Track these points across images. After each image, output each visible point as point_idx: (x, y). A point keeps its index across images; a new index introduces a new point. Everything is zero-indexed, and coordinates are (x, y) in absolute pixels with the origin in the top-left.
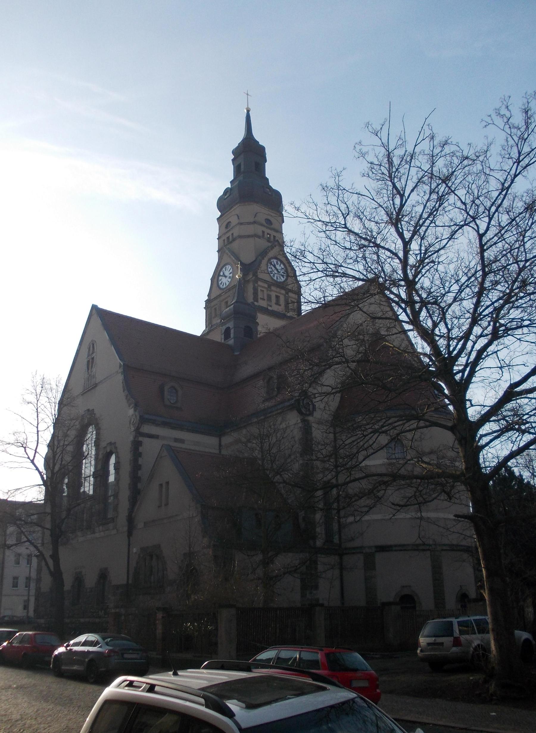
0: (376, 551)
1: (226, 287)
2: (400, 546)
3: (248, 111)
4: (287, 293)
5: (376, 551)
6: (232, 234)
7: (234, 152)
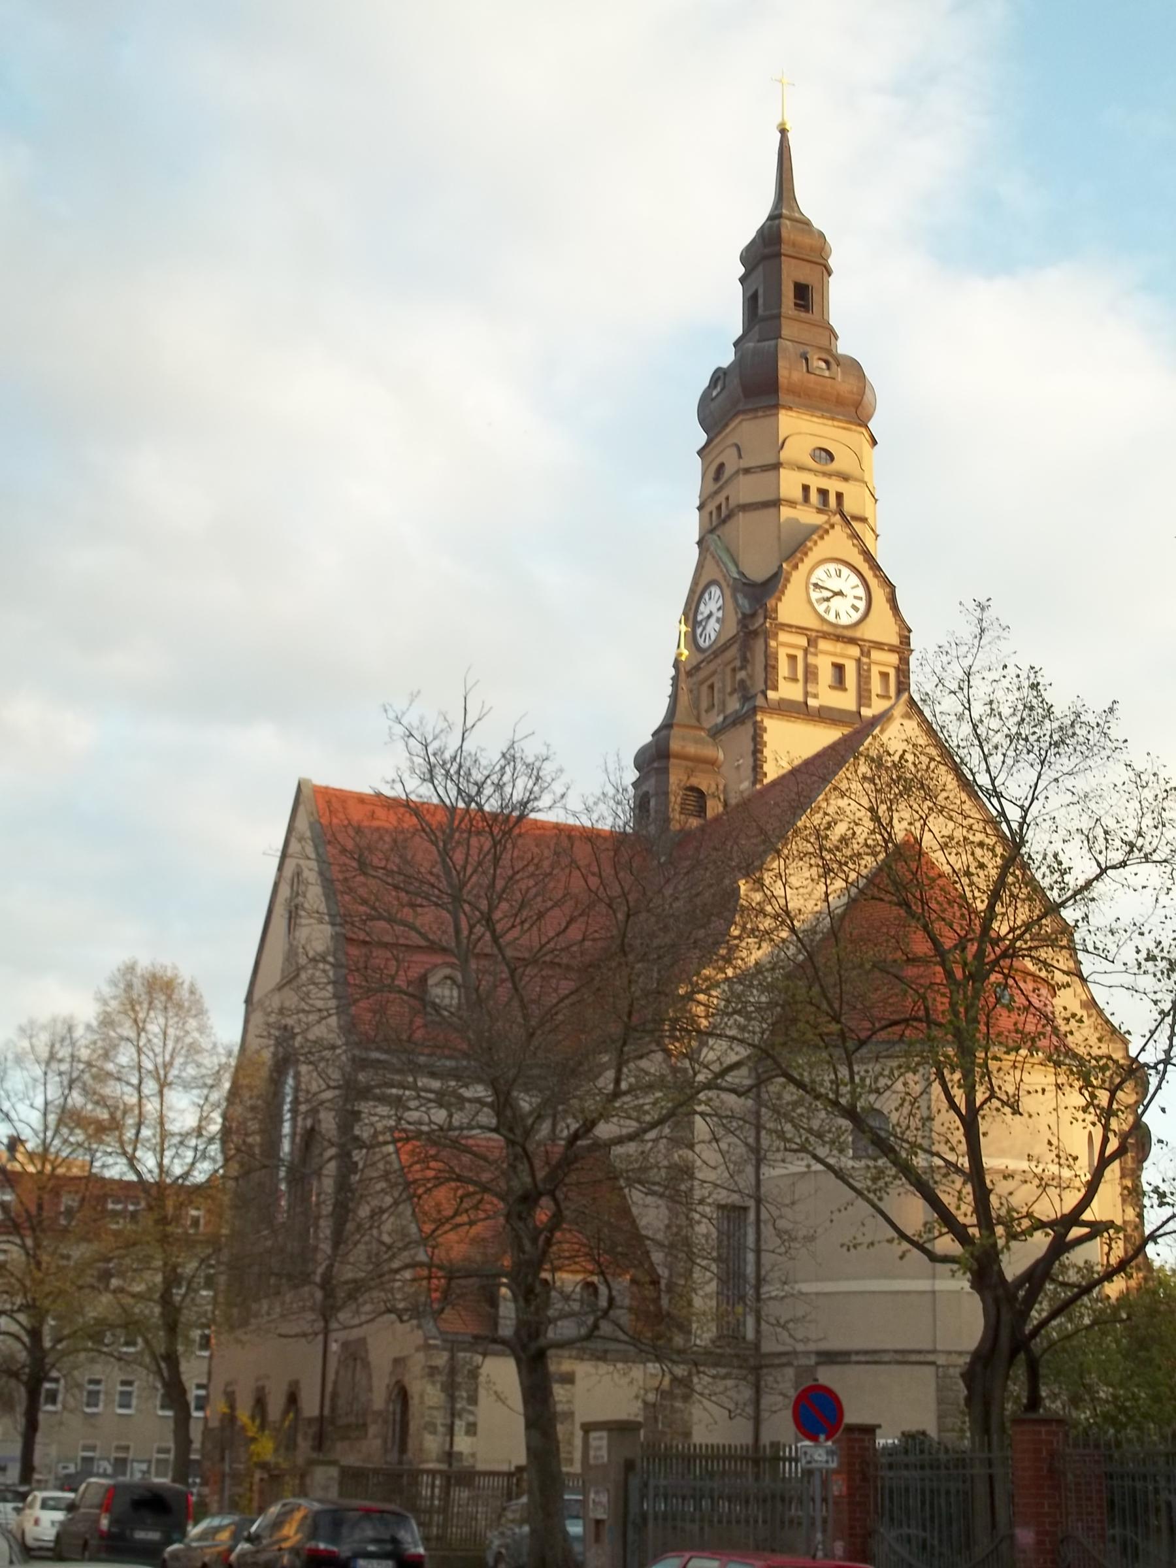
0: (818, 1364)
1: (711, 646)
2: (866, 1352)
3: (783, 132)
4: (866, 653)
5: (818, 1364)
6: (727, 499)
7: (744, 259)
